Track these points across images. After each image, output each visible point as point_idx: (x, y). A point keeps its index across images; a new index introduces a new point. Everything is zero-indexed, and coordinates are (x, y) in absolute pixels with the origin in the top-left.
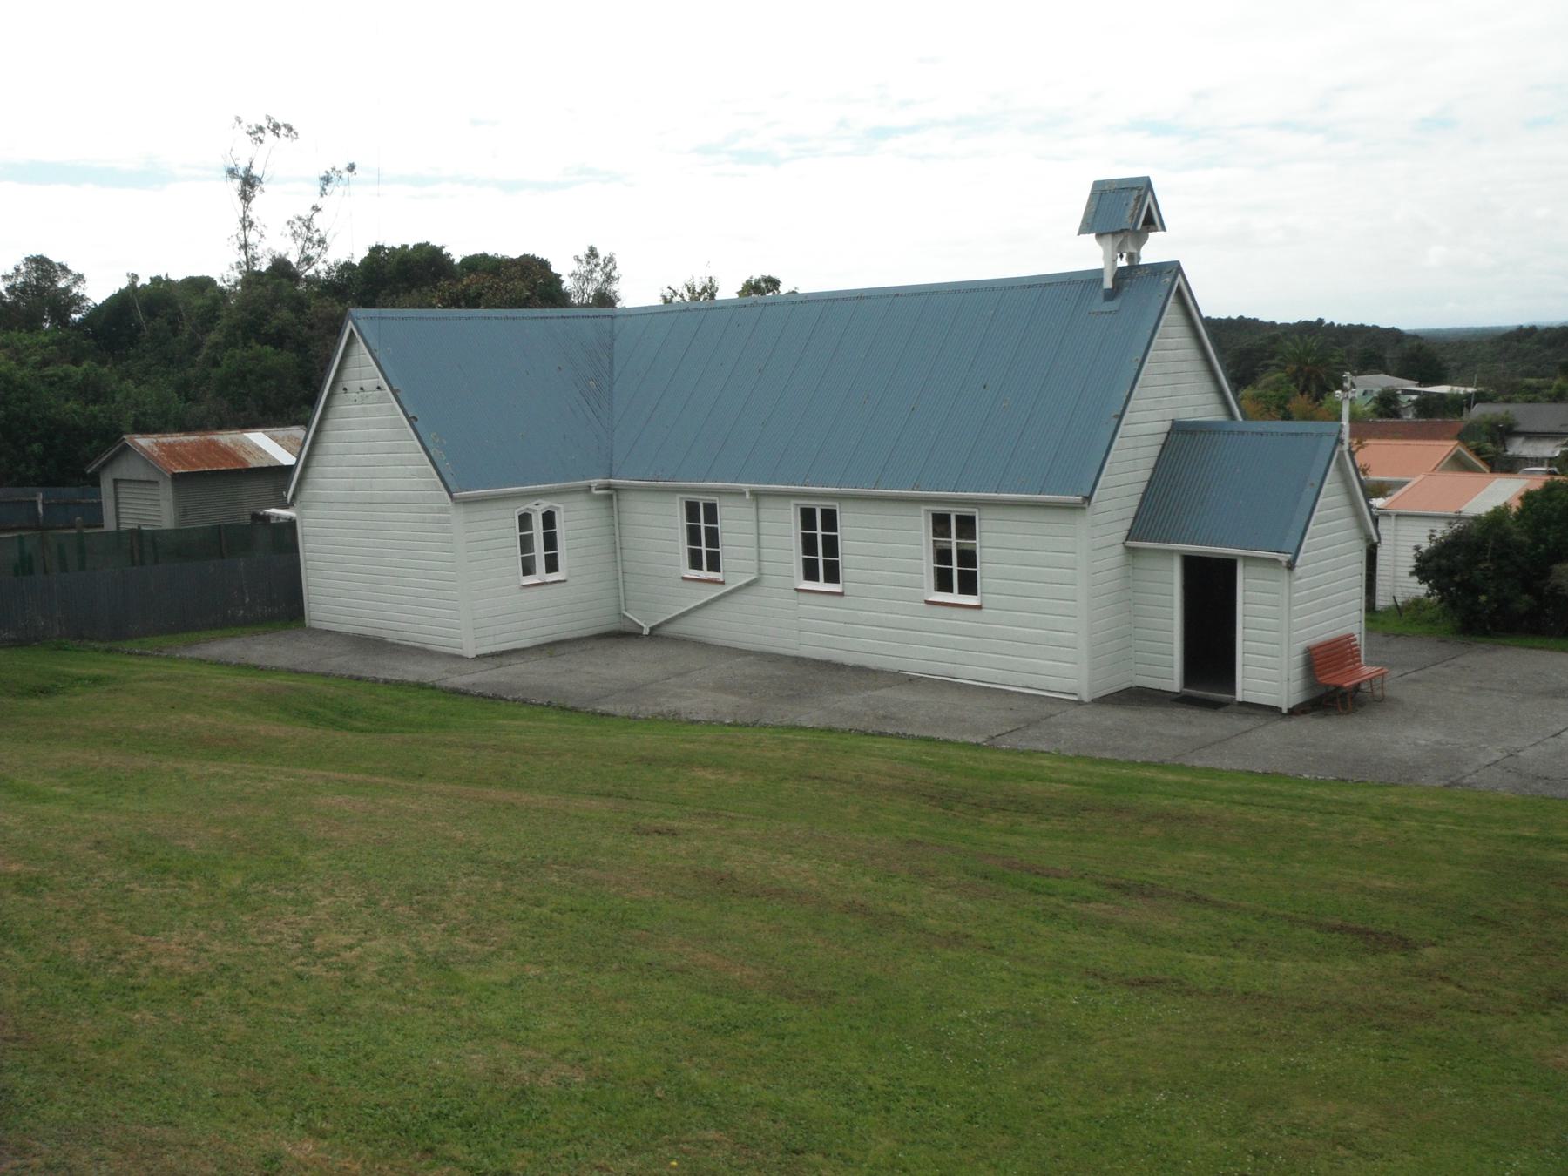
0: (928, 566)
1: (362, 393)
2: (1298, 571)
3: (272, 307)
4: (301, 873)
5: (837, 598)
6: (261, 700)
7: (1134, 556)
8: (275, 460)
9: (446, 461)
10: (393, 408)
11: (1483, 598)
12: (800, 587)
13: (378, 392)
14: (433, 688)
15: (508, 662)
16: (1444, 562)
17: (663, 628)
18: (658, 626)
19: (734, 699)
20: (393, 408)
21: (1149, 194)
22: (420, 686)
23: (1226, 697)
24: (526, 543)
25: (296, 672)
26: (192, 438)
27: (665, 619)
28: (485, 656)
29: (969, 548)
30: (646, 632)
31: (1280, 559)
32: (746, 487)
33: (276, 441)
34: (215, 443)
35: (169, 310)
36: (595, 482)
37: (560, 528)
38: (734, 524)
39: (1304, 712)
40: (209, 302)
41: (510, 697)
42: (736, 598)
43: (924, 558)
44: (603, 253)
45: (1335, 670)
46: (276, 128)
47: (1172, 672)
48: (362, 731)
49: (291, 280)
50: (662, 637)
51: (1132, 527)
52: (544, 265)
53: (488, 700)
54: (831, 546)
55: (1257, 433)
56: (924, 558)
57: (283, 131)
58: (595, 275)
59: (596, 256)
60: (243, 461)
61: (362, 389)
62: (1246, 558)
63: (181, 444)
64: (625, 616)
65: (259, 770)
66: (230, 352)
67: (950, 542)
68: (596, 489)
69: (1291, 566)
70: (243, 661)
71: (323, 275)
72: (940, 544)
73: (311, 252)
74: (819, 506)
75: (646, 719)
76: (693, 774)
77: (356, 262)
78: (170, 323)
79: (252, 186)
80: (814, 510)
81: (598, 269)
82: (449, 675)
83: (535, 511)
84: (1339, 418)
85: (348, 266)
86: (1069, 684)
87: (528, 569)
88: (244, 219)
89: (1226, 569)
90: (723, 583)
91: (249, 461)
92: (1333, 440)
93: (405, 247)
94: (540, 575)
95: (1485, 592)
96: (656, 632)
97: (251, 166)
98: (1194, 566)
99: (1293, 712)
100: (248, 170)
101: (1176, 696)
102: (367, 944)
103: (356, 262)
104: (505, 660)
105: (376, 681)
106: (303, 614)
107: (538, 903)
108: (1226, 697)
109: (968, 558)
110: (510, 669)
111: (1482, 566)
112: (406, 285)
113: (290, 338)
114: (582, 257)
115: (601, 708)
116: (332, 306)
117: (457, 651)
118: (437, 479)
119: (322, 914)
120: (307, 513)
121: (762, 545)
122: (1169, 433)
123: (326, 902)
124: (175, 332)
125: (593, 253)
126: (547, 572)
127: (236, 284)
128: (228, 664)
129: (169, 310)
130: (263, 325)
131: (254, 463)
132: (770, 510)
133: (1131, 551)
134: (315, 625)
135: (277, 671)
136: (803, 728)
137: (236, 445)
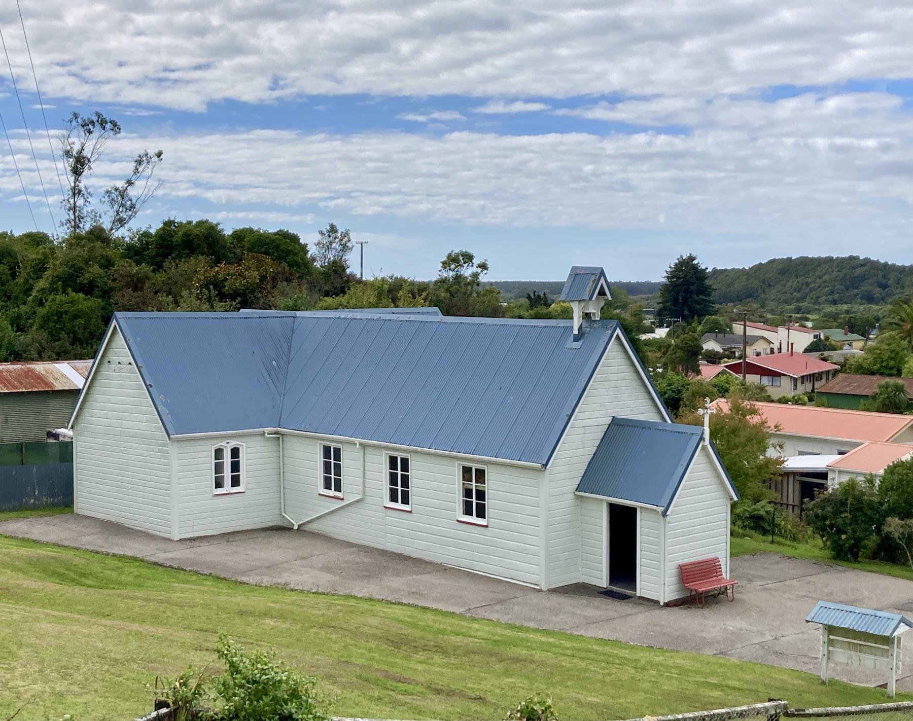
0: (459, 498)
1: (119, 366)
2: (668, 518)
3: (87, 263)
4: (15, 657)
5: (408, 514)
6: (31, 564)
7: (581, 501)
8: (74, 384)
9: (168, 414)
10: (138, 377)
11: (843, 537)
12: (387, 506)
13: (130, 366)
14: (142, 561)
15: (198, 545)
16: (820, 511)
17: (306, 526)
18: (304, 524)
19: (329, 577)
20: (138, 377)
21: (602, 277)
22: (134, 559)
23: (629, 592)
24: (219, 468)
25: (59, 546)
26: (16, 367)
27: (307, 520)
28: (186, 540)
29: (482, 489)
30: (296, 527)
31: (658, 510)
32: (357, 441)
33: (77, 370)
34: (32, 371)
35: (10, 260)
36: (267, 430)
37: (243, 459)
38: (350, 462)
39: (675, 605)
40: (40, 256)
41: (187, 569)
42: (352, 509)
43: (457, 493)
44: (341, 230)
45: (703, 580)
46: (103, 123)
47: (602, 575)
48: (90, 587)
49: (103, 242)
50: (305, 531)
51: (580, 483)
52: (294, 239)
53: (174, 570)
54: (405, 481)
55: (658, 429)
56: (457, 493)
57: (109, 126)
58: (334, 245)
59: (336, 232)
60: (47, 384)
61: (119, 363)
62: (641, 508)
63: (8, 371)
64: (283, 516)
65: (12, 608)
66: (51, 297)
67: (472, 485)
68: (268, 434)
69: (664, 514)
70: (26, 536)
71: (127, 239)
72: (468, 486)
73: (123, 215)
74: (399, 456)
75: (266, 587)
76: (263, 621)
77: (153, 231)
78: (10, 269)
79: (83, 165)
80: (397, 457)
81: (337, 240)
82: (157, 552)
83: (226, 447)
84: (703, 425)
85: (146, 234)
86: (534, 578)
87: (219, 484)
88: (74, 187)
89: (632, 512)
90: (343, 499)
91: (55, 384)
92: (699, 437)
93: (190, 223)
94: (227, 487)
95: (845, 533)
96: (302, 528)
97: (83, 149)
98: (613, 508)
99: (668, 605)
100: (80, 152)
101: (601, 590)
102: (32, 686)
103: (153, 231)
104: (196, 544)
105: (108, 554)
106: (73, 503)
107: (120, 676)
108: (629, 592)
109: (481, 495)
110: (198, 549)
111: (843, 515)
112: (187, 251)
113: (98, 287)
114: (324, 231)
115: (240, 579)
116: (130, 266)
117: (168, 536)
118: (161, 424)
119: (16, 674)
120: (79, 435)
121: (366, 477)
122: (609, 425)
123: (20, 669)
124: (14, 276)
125: (333, 229)
126: (232, 486)
127: (63, 242)
128: (16, 538)
129: (10, 260)
130: (79, 277)
131: (59, 387)
132: (371, 455)
133: (578, 497)
134: (81, 512)
135: (47, 544)
136: (355, 597)
137: (47, 372)
